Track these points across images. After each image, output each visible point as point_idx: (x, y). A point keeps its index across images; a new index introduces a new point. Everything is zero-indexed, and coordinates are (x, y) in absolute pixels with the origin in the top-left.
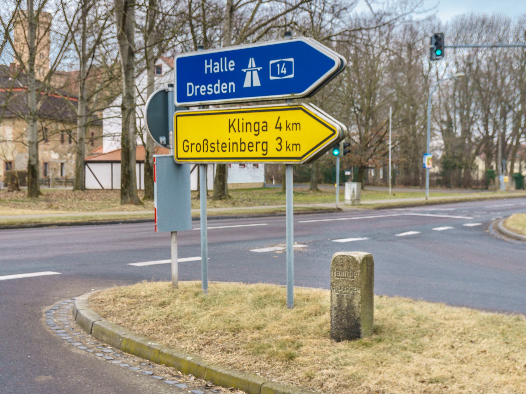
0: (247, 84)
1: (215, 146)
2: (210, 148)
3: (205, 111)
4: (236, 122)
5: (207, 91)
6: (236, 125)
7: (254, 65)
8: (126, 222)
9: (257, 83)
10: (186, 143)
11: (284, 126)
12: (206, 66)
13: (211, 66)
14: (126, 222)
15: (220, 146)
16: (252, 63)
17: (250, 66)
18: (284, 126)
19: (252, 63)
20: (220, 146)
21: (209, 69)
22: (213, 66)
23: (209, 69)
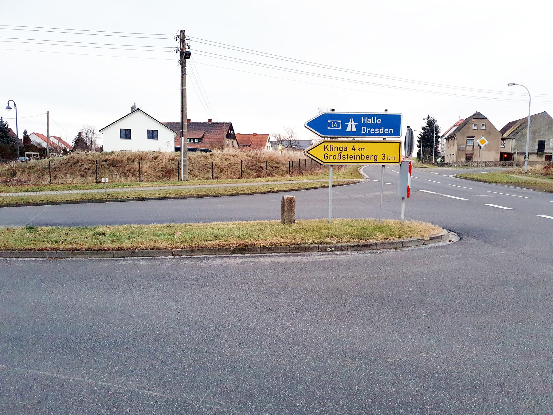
0: (348, 129)
1: (346, 157)
2: (342, 158)
3: (332, 140)
4: (329, 146)
5: (375, 131)
6: (328, 147)
7: (353, 122)
8: (56, 203)
9: (354, 129)
10: (326, 155)
11: (356, 149)
12: (363, 120)
13: (366, 120)
14: (56, 203)
15: (349, 157)
16: (352, 121)
17: (350, 122)
18: (356, 149)
19: (352, 121)
20: (349, 157)
21: (364, 121)
22: (367, 120)
23: (364, 121)
